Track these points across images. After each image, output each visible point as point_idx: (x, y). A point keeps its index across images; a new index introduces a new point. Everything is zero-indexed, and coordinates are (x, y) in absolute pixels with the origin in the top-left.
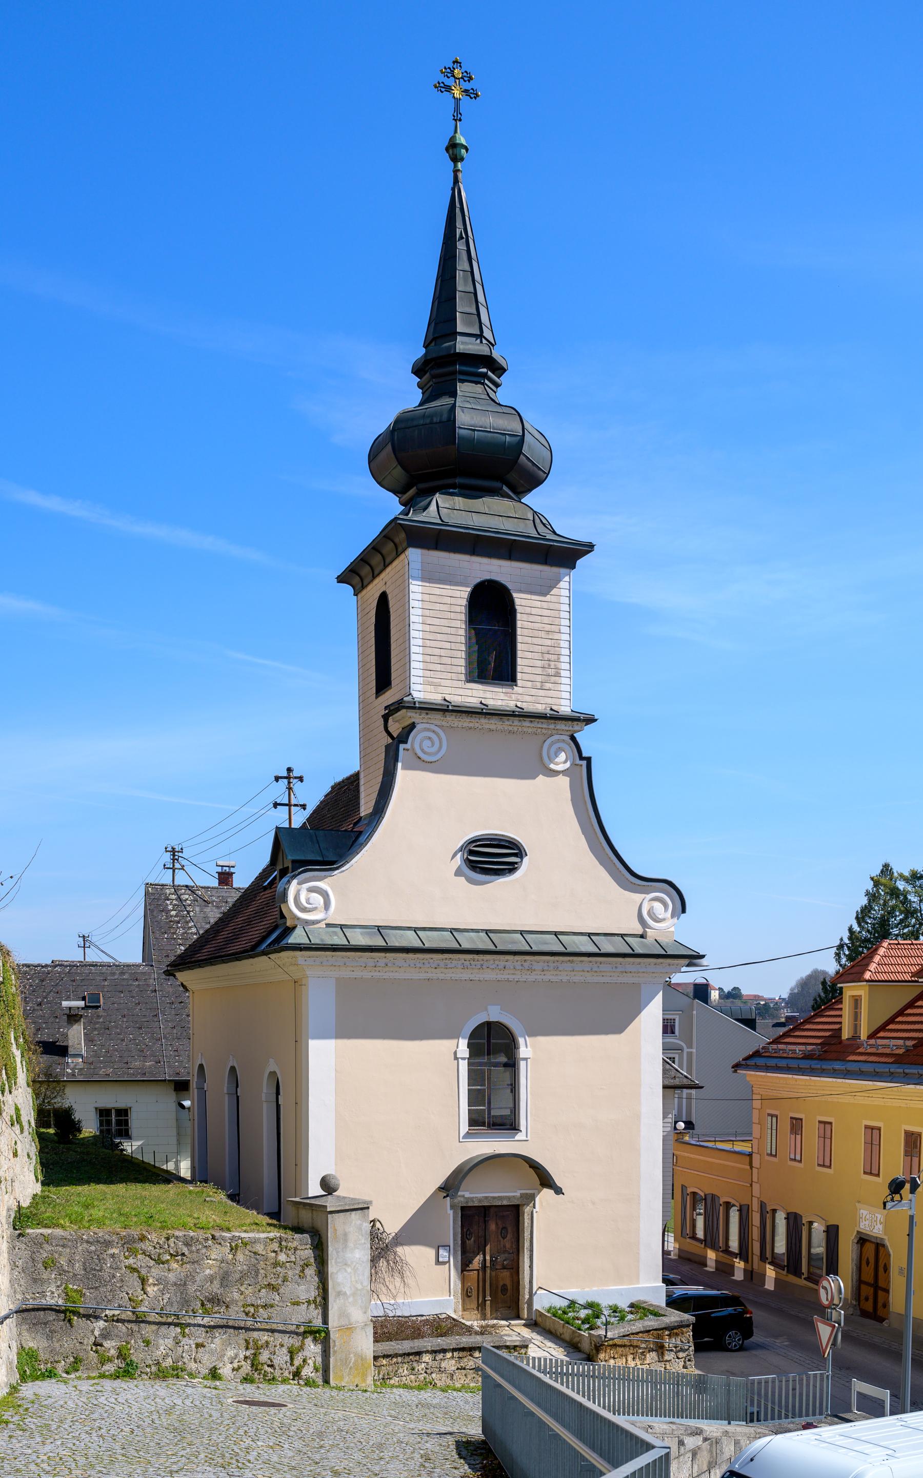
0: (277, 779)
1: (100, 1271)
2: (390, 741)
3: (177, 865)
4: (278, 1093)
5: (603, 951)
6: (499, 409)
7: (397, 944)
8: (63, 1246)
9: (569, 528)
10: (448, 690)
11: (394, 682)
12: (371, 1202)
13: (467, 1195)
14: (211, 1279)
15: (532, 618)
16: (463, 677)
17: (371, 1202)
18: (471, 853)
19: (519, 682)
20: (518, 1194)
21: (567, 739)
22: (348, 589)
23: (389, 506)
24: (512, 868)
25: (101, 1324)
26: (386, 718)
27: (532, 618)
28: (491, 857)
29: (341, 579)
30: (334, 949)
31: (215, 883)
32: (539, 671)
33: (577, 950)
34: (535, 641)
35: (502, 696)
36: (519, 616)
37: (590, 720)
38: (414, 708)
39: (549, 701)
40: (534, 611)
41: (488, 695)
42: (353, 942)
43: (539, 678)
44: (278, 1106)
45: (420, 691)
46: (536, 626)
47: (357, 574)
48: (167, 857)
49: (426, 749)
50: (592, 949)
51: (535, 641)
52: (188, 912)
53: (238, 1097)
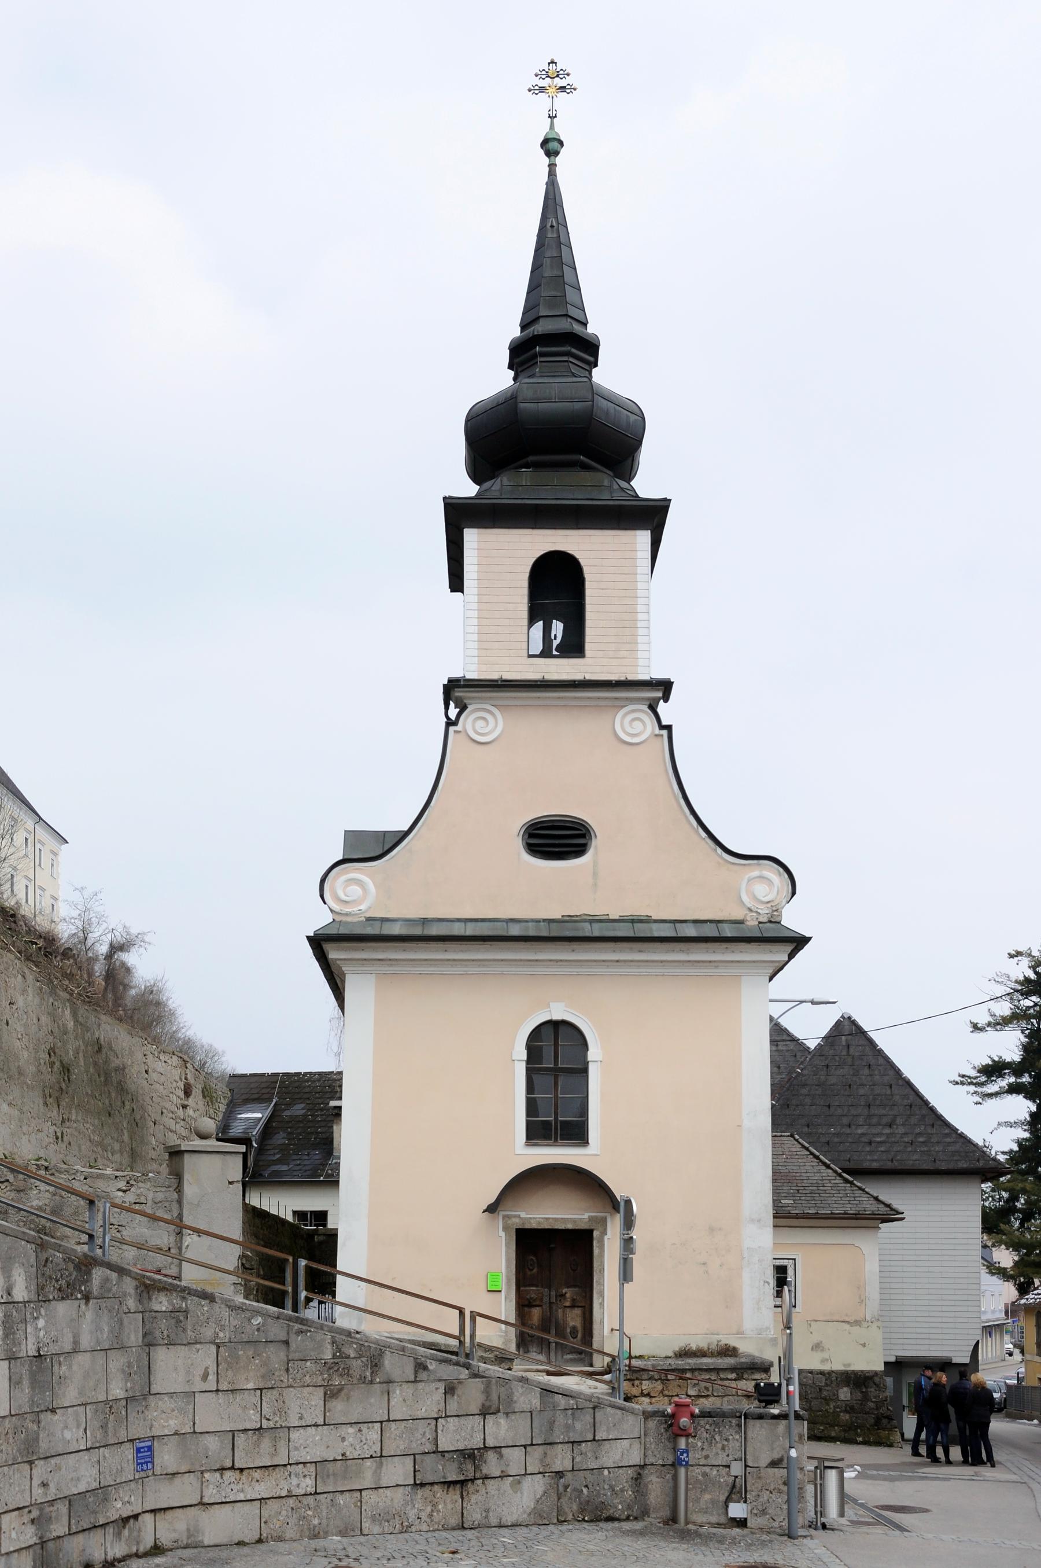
18: (531, 836)
20: (586, 1216)
24: (580, 850)
36: (587, 585)
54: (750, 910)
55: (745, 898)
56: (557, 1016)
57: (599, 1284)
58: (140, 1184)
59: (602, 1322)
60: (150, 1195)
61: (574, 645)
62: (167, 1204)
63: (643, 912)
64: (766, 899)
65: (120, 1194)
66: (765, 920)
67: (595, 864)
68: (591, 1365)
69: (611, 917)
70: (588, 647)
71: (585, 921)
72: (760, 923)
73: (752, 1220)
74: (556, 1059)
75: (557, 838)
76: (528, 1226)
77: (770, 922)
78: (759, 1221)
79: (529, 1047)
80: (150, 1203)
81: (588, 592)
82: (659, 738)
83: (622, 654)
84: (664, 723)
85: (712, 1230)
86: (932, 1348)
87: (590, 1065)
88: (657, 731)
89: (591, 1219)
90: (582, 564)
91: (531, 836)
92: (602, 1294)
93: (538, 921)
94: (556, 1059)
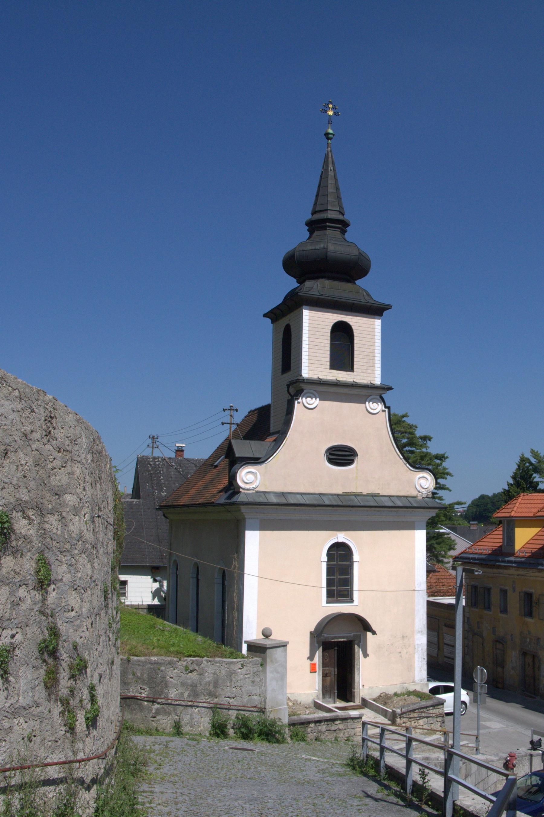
0: (224, 410)
1: (156, 678)
2: (290, 397)
3: (155, 446)
4: (198, 574)
5: (396, 505)
6: (346, 244)
7: (292, 502)
8: (139, 665)
9: (379, 297)
10: (320, 373)
11: (292, 368)
12: (288, 643)
13: (325, 635)
14: (210, 683)
15: (361, 339)
16: (328, 367)
17: (288, 643)
18: (330, 454)
19: (355, 370)
20: (352, 635)
21: (378, 397)
22: (268, 321)
23: (292, 283)
24: (350, 462)
25: (157, 706)
26: (288, 386)
27: (361, 339)
28: (341, 456)
29: (265, 316)
30: (260, 504)
31: (173, 455)
32: (365, 364)
33: (384, 505)
34: (363, 350)
35: (347, 376)
36: (355, 338)
37: (390, 389)
38: (304, 382)
39: (370, 379)
40: (362, 335)
41: (340, 376)
42: (270, 501)
43: (365, 368)
44: (198, 580)
45: (306, 373)
46: (363, 343)
47: (275, 315)
48: (150, 441)
49: (309, 403)
50: (391, 504)
51: (363, 350)
52: (160, 471)
53: (177, 575)
54: (419, 492)
55: (418, 487)
56: (340, 540)
57: (357, 665)
58: (248, 665)
59: (359, 682)
60: (252, 669)
61: (349, 366)
62: (258, 673)
63: (377, 491)
64: (425, 487)
65: (240, 670)
66: (424, 496)
67: (356, 467)
68: (354, 702)
69: (363, 494)
70: (355, 367)
71: (352, 495)
72: (423, 498)
73: (419, 632)
74: (340, 562)
75: (341, 456)
76: (327, 640)
77: (427, 497)
78: (422, 632)
79: (328, 555)
80: (252, 673)
81: (356, 341)
82: (384, 413)
83: (369, 371)
84: (387, 405)
85: (403, 637)
86: (366, 378)
87: (354, 563)
88: (384, 409)
89: (354, 635)
90: (355, 334)
91: (330, 454)
92: (359, 670)
93: (332, 495)
94: (340, 562)
